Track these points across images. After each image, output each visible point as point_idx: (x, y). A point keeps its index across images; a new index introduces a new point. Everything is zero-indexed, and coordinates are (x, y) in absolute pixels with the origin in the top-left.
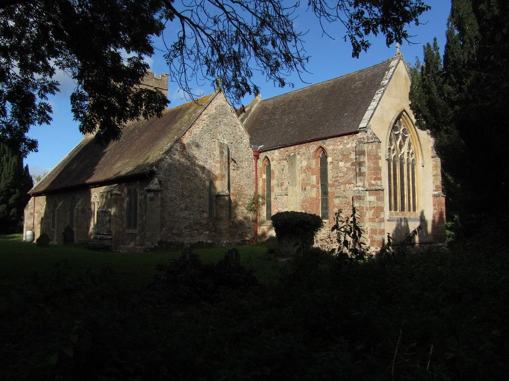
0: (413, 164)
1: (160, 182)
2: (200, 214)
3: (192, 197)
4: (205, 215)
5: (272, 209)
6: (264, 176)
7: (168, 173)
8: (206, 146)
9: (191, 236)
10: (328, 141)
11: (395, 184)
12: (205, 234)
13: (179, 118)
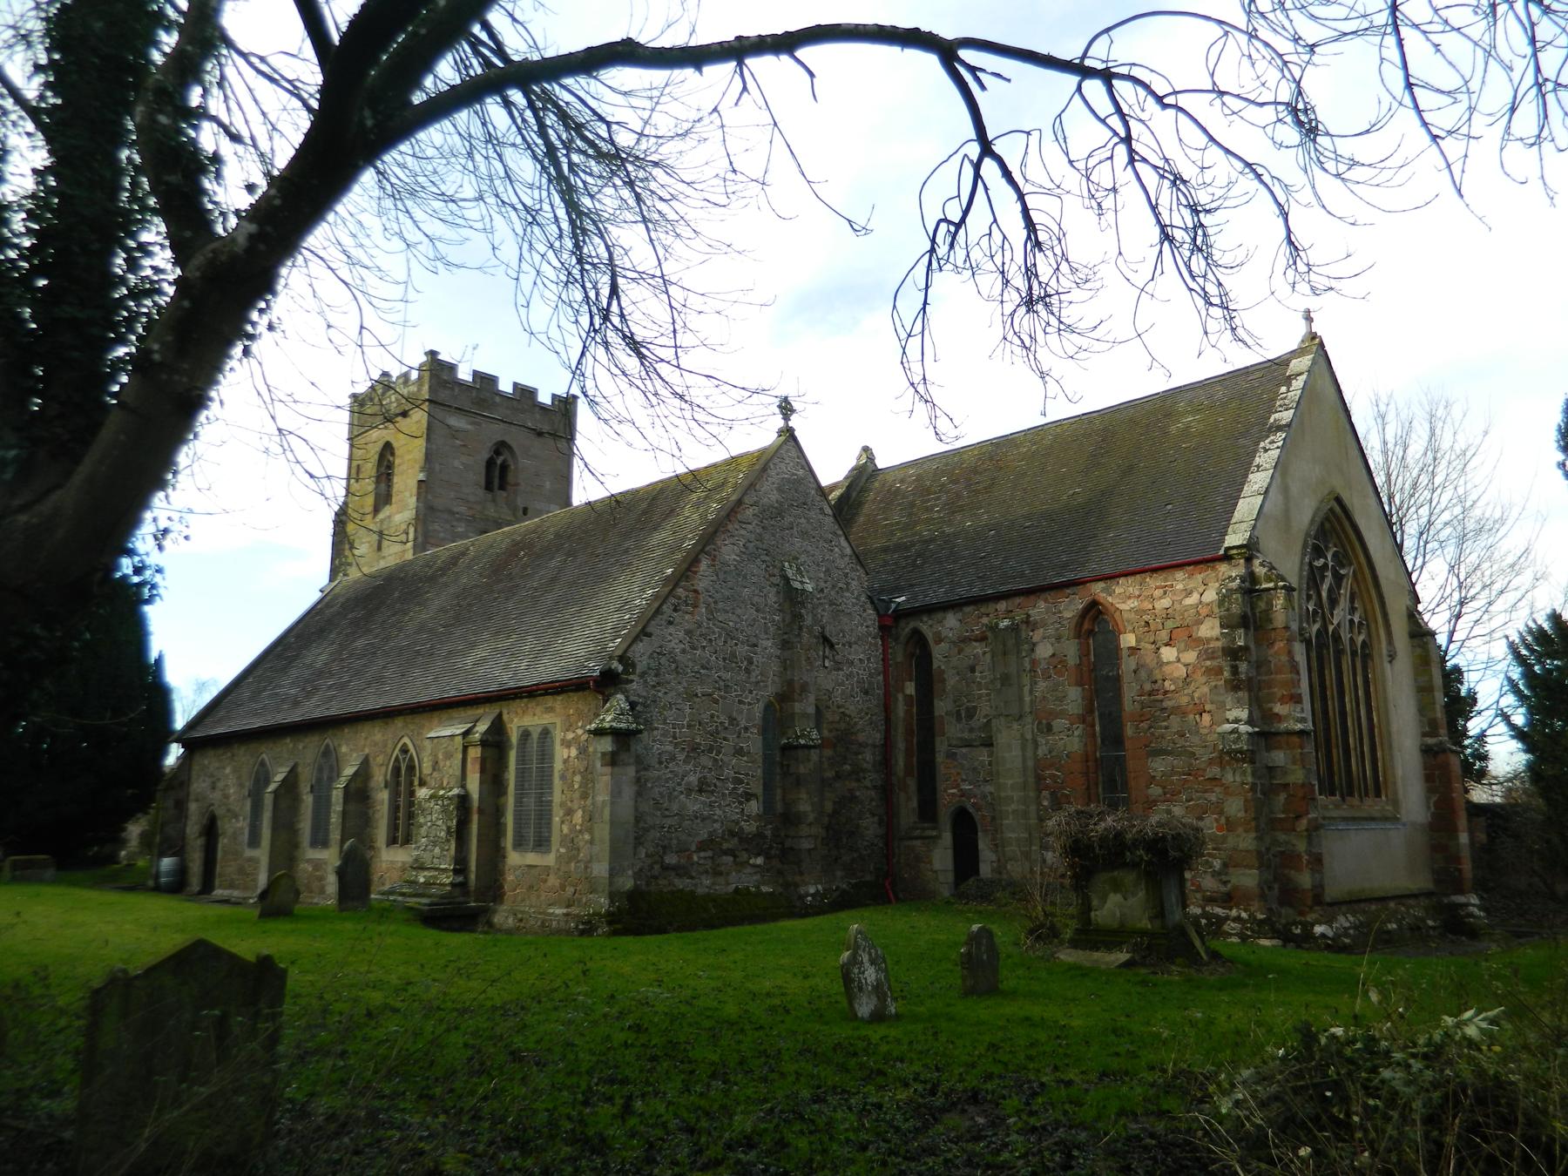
0: (1366, 654)
2: (741, 803)
3: (719, 753)
4: (754, 807)
5: (941, 786)
6: (910, 688)
7: (652, 680)
8: (756, 599)
10: (1124, 587)
11: (1359, 718)
12: (754, 866)
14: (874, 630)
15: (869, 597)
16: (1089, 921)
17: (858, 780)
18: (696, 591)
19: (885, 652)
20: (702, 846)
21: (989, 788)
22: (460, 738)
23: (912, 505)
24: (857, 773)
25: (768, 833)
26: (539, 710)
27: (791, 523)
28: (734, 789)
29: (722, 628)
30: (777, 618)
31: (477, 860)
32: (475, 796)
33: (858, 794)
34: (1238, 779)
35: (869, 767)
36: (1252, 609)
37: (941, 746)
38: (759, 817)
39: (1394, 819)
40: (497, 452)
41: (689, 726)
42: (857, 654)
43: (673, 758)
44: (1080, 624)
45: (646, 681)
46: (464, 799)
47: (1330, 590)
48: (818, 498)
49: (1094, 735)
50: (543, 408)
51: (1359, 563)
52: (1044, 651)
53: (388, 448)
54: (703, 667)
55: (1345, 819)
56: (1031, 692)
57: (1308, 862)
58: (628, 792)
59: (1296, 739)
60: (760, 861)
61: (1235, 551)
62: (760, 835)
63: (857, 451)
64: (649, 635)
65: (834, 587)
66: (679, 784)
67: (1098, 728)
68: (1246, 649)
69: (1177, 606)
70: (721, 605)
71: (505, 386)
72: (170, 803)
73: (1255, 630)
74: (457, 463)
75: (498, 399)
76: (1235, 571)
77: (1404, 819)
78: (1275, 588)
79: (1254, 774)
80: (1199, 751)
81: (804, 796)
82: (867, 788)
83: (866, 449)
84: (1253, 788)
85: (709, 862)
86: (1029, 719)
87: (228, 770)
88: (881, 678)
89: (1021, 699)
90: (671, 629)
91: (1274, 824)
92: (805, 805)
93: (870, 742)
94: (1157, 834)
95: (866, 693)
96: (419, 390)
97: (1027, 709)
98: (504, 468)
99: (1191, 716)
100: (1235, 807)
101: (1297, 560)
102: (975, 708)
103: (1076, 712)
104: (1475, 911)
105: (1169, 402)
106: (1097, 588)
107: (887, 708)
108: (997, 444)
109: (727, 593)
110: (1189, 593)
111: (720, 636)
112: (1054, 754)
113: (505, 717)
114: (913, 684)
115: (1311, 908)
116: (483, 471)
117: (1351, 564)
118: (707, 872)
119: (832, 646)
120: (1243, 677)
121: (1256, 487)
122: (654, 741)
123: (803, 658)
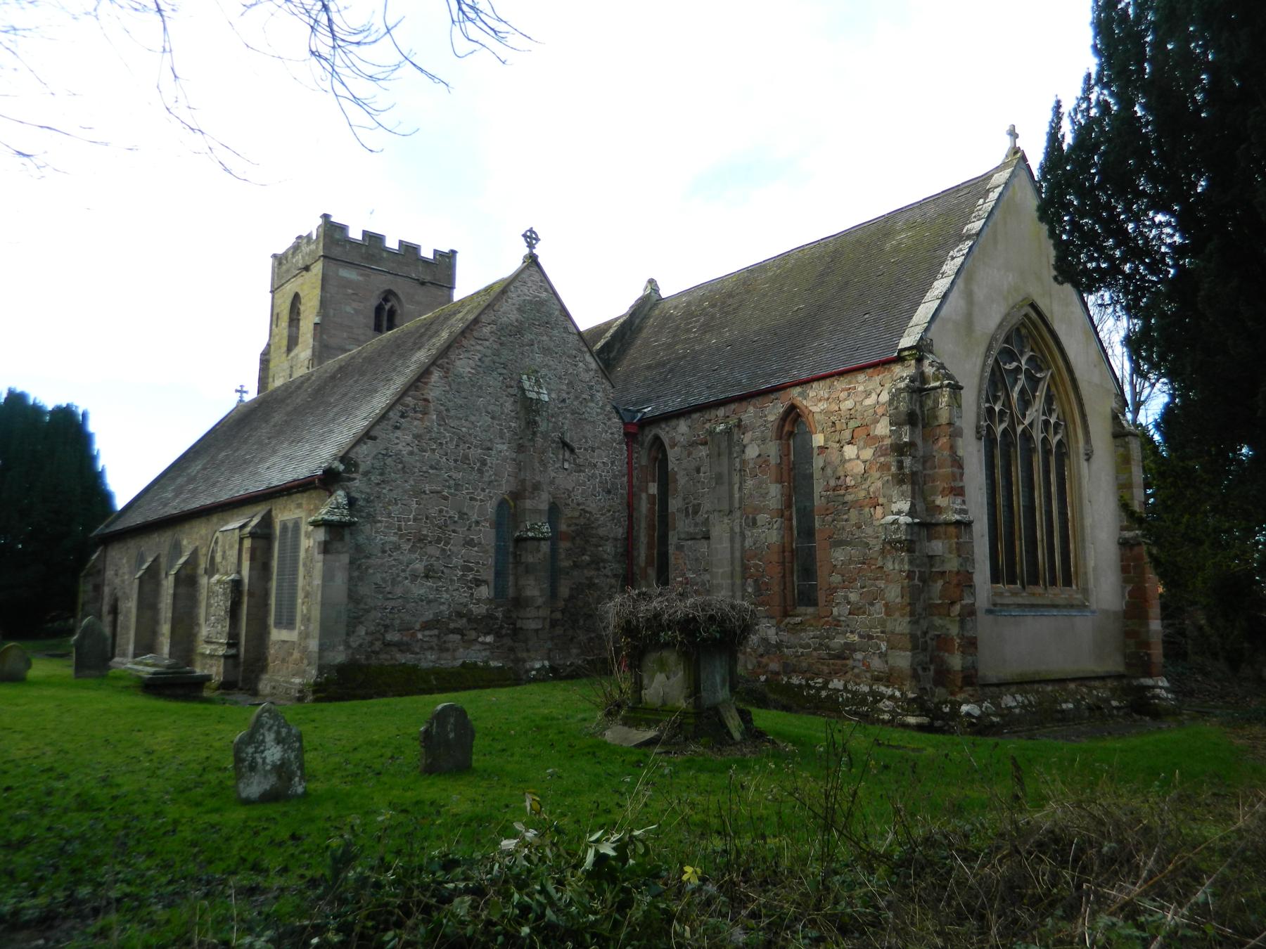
0: (1063, 452)
1: (352, 502)
3: (447, 543)
4: (484, 592)
6: (653, 489)
8: (490, 408)
9: (443, 649)
12: (483, 643)
13: (431, 337)
14: (619, 436)
15: (615, 408)
16: (640, 700)
17: (598, 569)
18: (426, 400)
19: (630, 457)
20: (426, 626)
21: (707, 577)
22: (237, 531)
23: (678, 328)
24: (597, 562)
25: (499, 615)
26: (293, 506)
27: (532, 340)
28: (463, 575)
29: (454, 433)
30: (513, 425)
31: (246, 636)
32: (246, 581)
33: (596, 581)
34: (897, 567)
35: (610, 557)
36: (922, 406)
37: (673, 539)
38: (490, 601)
39: (1082, 607)
40: (386, 300)
41: (415, 520)
42: (601, 457)
43: (397, 547)
44: (781, 427)
45: (370, 479)
46: (237, 584)
47: (1022, 392)
48: (562, 318)
49: (791, 528)
50: (425, 261)
51: (1057, 367)
52: (752, 452)
53: (296, 298)
54: (432, 467)
55: (1019, 606)
56: (740, 489)
57: (960, 645)
58: (340, 579)
59: (952, 530)
60: (489, 639)
61: (906, 353)
62: (490, 616)
63: (644, 283)
64: (374, 438)
65: (577, 398)
66: (404, 571)
67: (794, 522)
68: (912, 444)
69: (858, 406)
70: (453, 413)
71: (392, 243)
72: (89, 587)
73: (923, 427)
74: (348, 309)
75: (385, 255)
76: (904, 372)
77: (1094, 607)
78: (941, 387)
79: (911, 562)
80: (872, 542)
81: (532, 582)
82: (607, 576)
83: (651, 281)
84: (910, 575)
85: (435, 640)
86: (738, 514)
87: (125, 561)
88: (625, 479)
89: (731, 496)
90: (398, 433)
91: (931, 609)
92: (534, 589)
93: (612, 535)
94: (688, 615)
95: (609, 492)
96: (317, 248)
97: (737, 505)
98: (392, 313)
99: (867, 509)
100: (893, 593)
101: (979, 362)
102: (699, 505)
103: (775, 507)
104: (1163, 693)
105: (890, 223)
106: (796, 391)
107: (631, 507)
108: (752, 270)
109: (460, 402)
110: (868, 395)
111: (452, 440)
112: (757, 545)
113: (274, 513)
114: (656, 485)
115: (961, 688)
116: (373, 315)
117: (1049, 368)
118: (431, 648)
119: (572, 450)
120: (907, 471)
121: (936, 292)
122: (376, 532)
123: (536, 461)
